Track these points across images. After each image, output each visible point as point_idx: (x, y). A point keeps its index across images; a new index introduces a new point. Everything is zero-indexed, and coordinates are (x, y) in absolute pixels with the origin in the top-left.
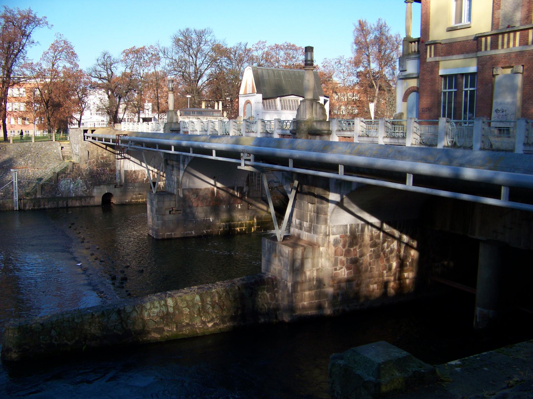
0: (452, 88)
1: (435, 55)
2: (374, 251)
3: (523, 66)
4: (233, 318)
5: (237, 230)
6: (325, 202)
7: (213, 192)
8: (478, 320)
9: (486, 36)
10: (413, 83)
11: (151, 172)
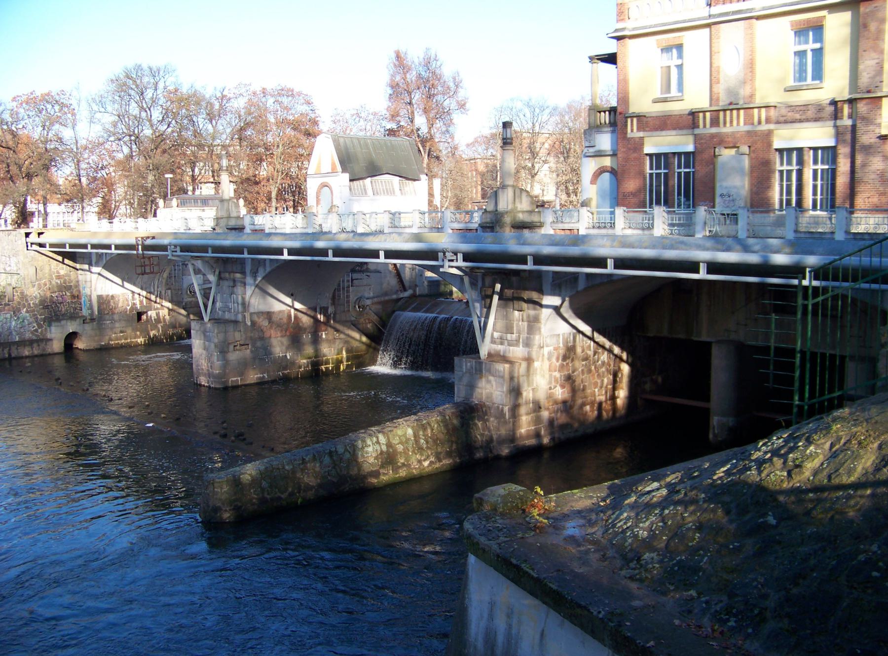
0: (661, 169)
1: (639, 129)
2: (586, 365)
3: (749, 147)
4: (449, 454)
5: (322, 370)
6: (538, 307)
7: (289, 316)
8: (716, 431)
9: (704, 112)
10: (607, 162)
11: (136, 296)
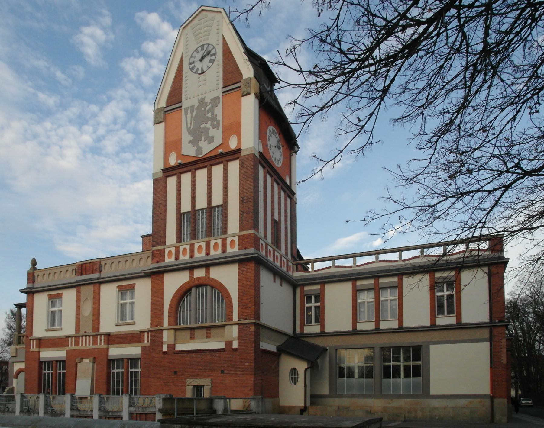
9: (72, 337)
